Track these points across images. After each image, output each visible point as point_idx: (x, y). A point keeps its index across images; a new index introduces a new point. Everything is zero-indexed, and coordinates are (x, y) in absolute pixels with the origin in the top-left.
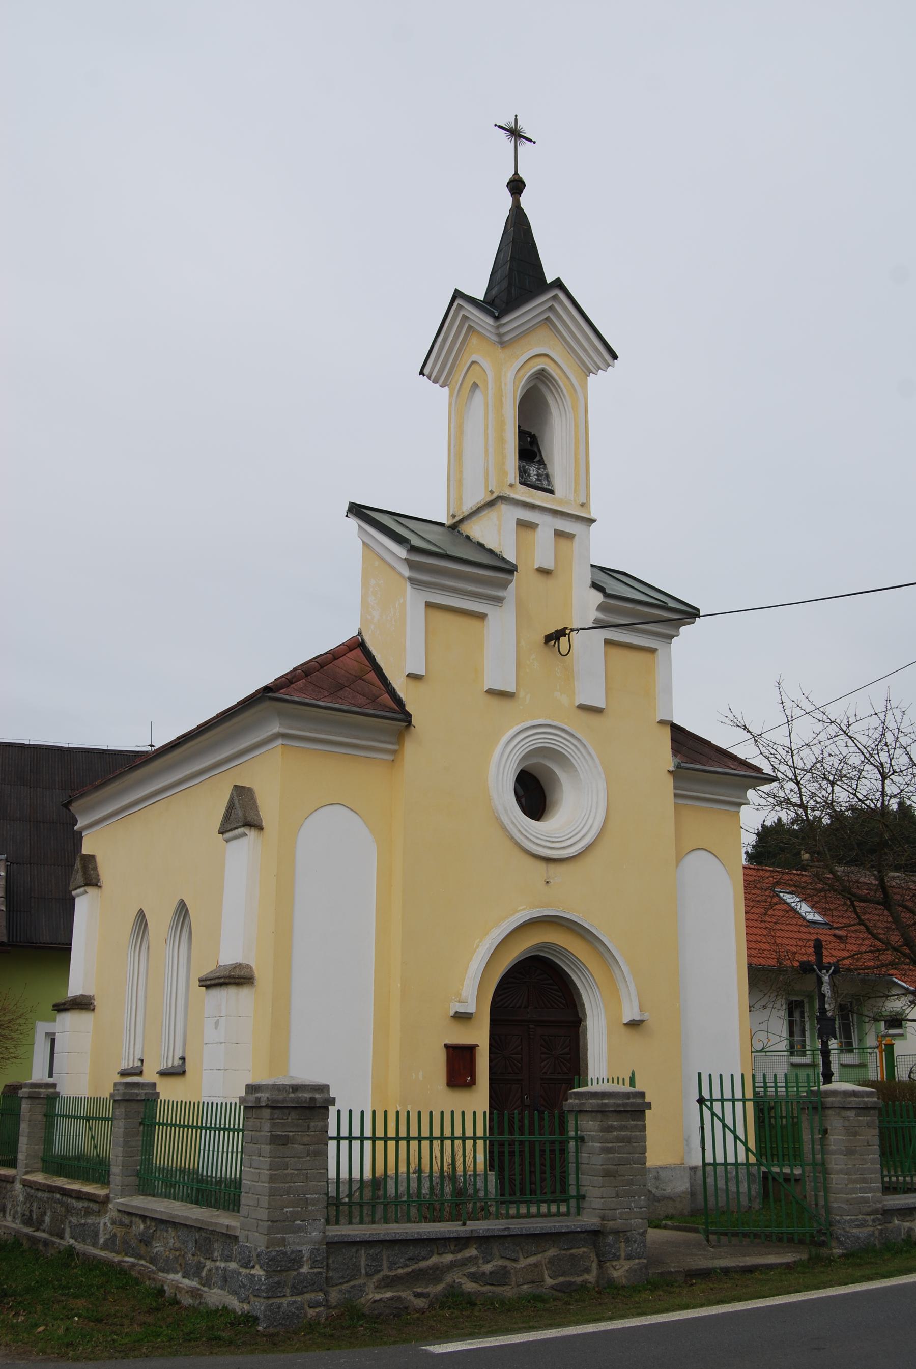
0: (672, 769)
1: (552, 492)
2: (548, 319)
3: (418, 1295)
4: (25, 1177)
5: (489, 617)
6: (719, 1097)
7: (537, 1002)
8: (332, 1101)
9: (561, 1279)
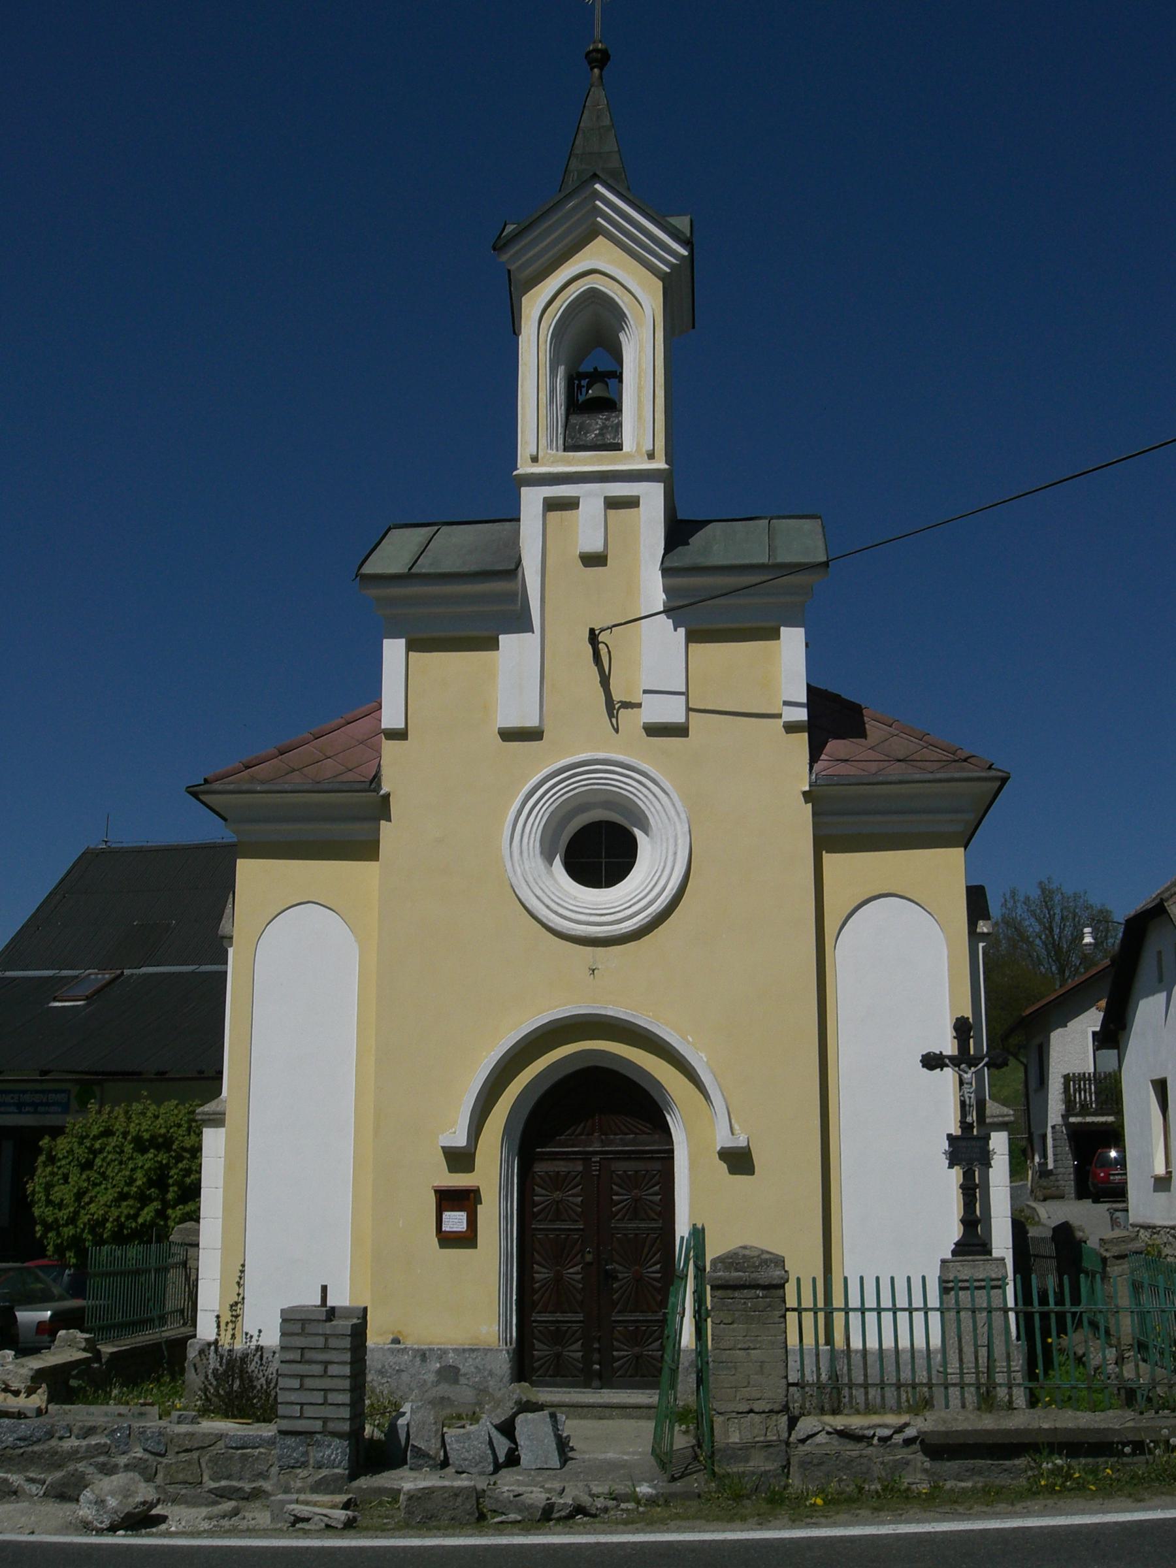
3: (31, 1480)
6: (890, 1306)
9: (223, 1483)
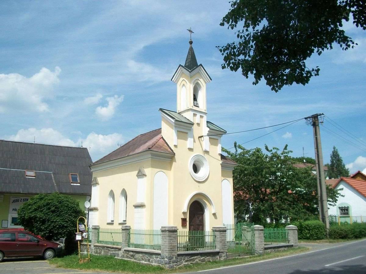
0: (221, 163)
1: (199, 107)
2: (199, 72)
4: (95, 244)
5: (189, 133)
7: (197, 208)
8: (178, 229)
